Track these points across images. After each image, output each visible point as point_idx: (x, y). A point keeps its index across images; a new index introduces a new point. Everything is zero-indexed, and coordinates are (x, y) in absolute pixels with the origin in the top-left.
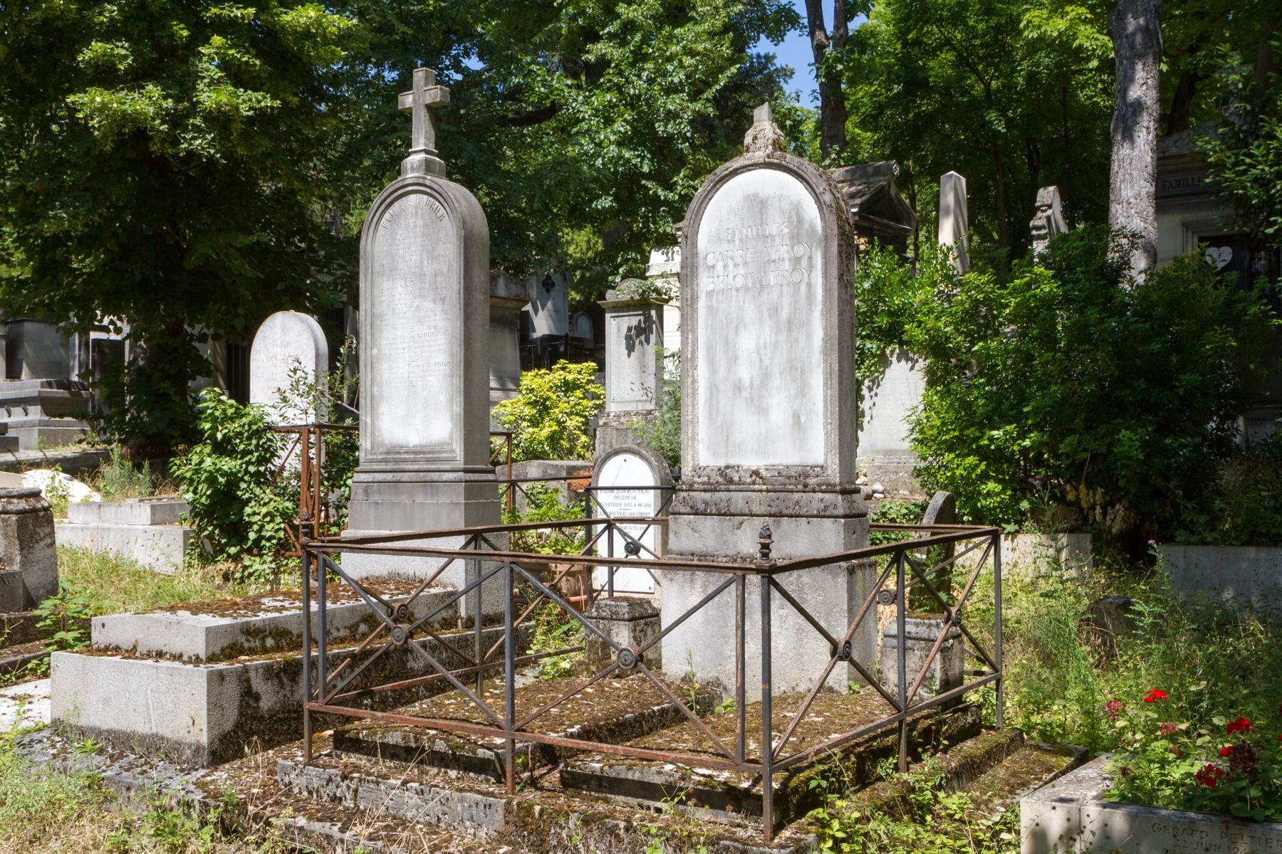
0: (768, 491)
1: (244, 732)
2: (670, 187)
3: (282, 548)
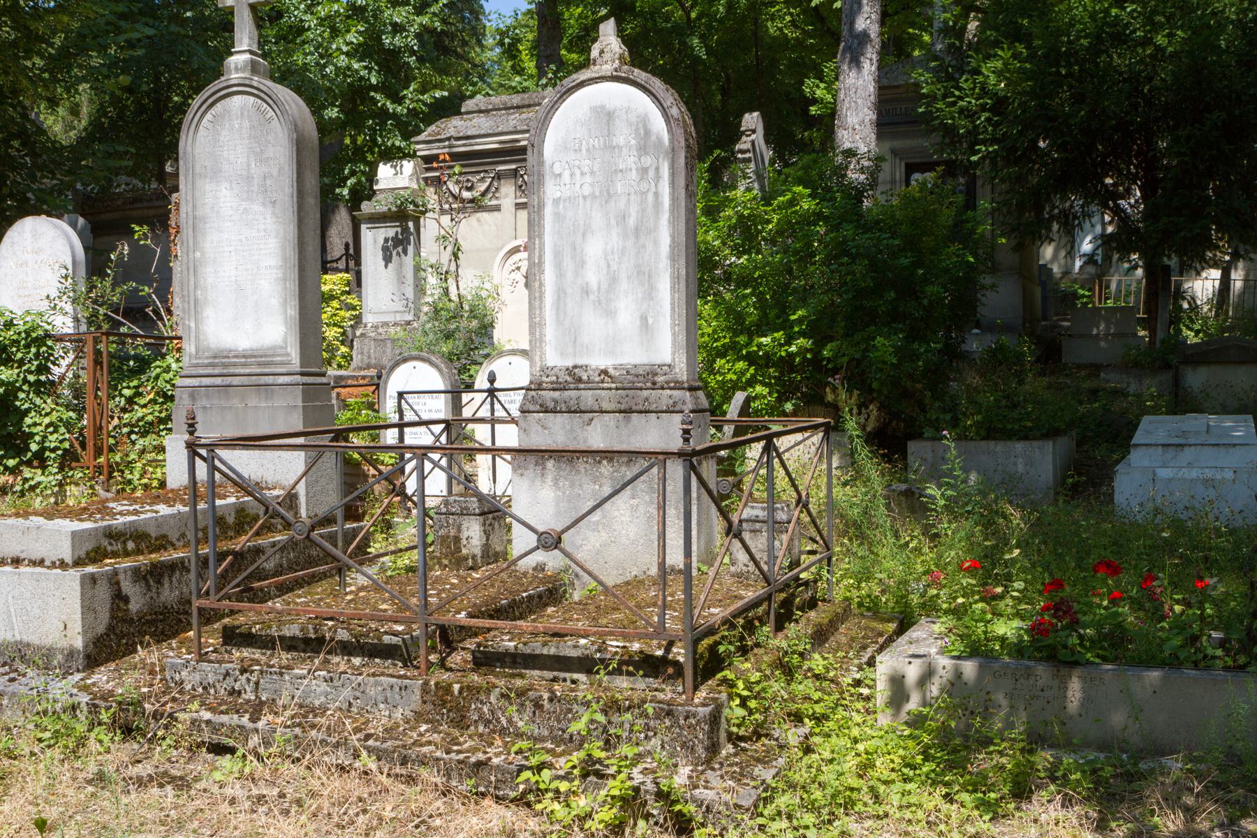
0: (617, 389)
1: (115, 634)
2: (399, 100)
3: (69, 459)
